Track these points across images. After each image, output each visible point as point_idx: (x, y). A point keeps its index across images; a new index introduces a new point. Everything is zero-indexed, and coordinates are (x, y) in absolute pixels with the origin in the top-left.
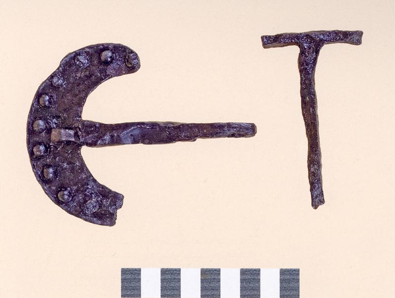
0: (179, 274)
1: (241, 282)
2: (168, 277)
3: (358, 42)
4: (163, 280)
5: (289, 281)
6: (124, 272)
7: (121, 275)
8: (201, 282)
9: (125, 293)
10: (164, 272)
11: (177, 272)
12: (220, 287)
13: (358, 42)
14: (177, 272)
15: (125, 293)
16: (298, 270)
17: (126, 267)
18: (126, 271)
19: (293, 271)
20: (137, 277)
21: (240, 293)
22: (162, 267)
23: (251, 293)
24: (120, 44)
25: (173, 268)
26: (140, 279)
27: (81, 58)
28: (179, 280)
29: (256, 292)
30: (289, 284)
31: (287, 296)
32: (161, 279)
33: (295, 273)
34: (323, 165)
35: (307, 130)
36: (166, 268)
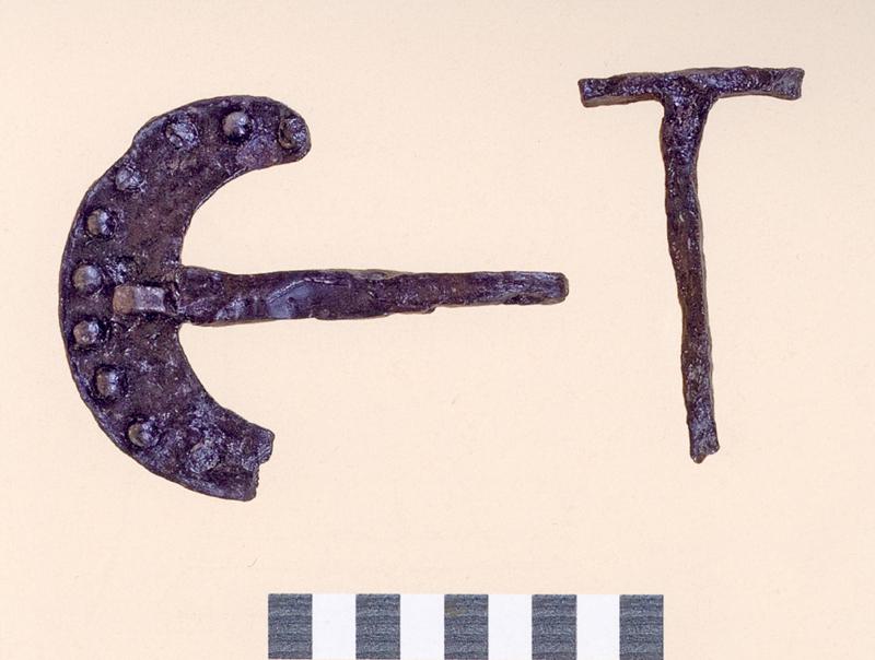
0: (397, 607)
1: (534, 625)
2: (372, 613)
3: (794, 94)
4: (360, 621)
5: (639, 623)
6: (275, 601)
7: (267, 609)
8: (446, 625)
9: (276, 648)
10: (363, 602)
11: (392, 602)
12: (487, 635)
13: (794, 94)
14: (392, 602)
15: (276, 648)
16: (661, 599)
17: (279, 592)
18: (280, 600)
19: (648, 600)
20: (303, 614)
21: (531, 649)
22: (360, 592)
23: (556, 648)
24: (265, 98)
25: (383, 593)
26: (311, 618)
27: (180, 129)
28: (397, 621)
29: (566, 648)
30: (640, 628)
31: (636, 655)
32: (357, 618)
33: (653, 606)
34: (715, 366)
35: (680, 287)
36: (368, 593)
